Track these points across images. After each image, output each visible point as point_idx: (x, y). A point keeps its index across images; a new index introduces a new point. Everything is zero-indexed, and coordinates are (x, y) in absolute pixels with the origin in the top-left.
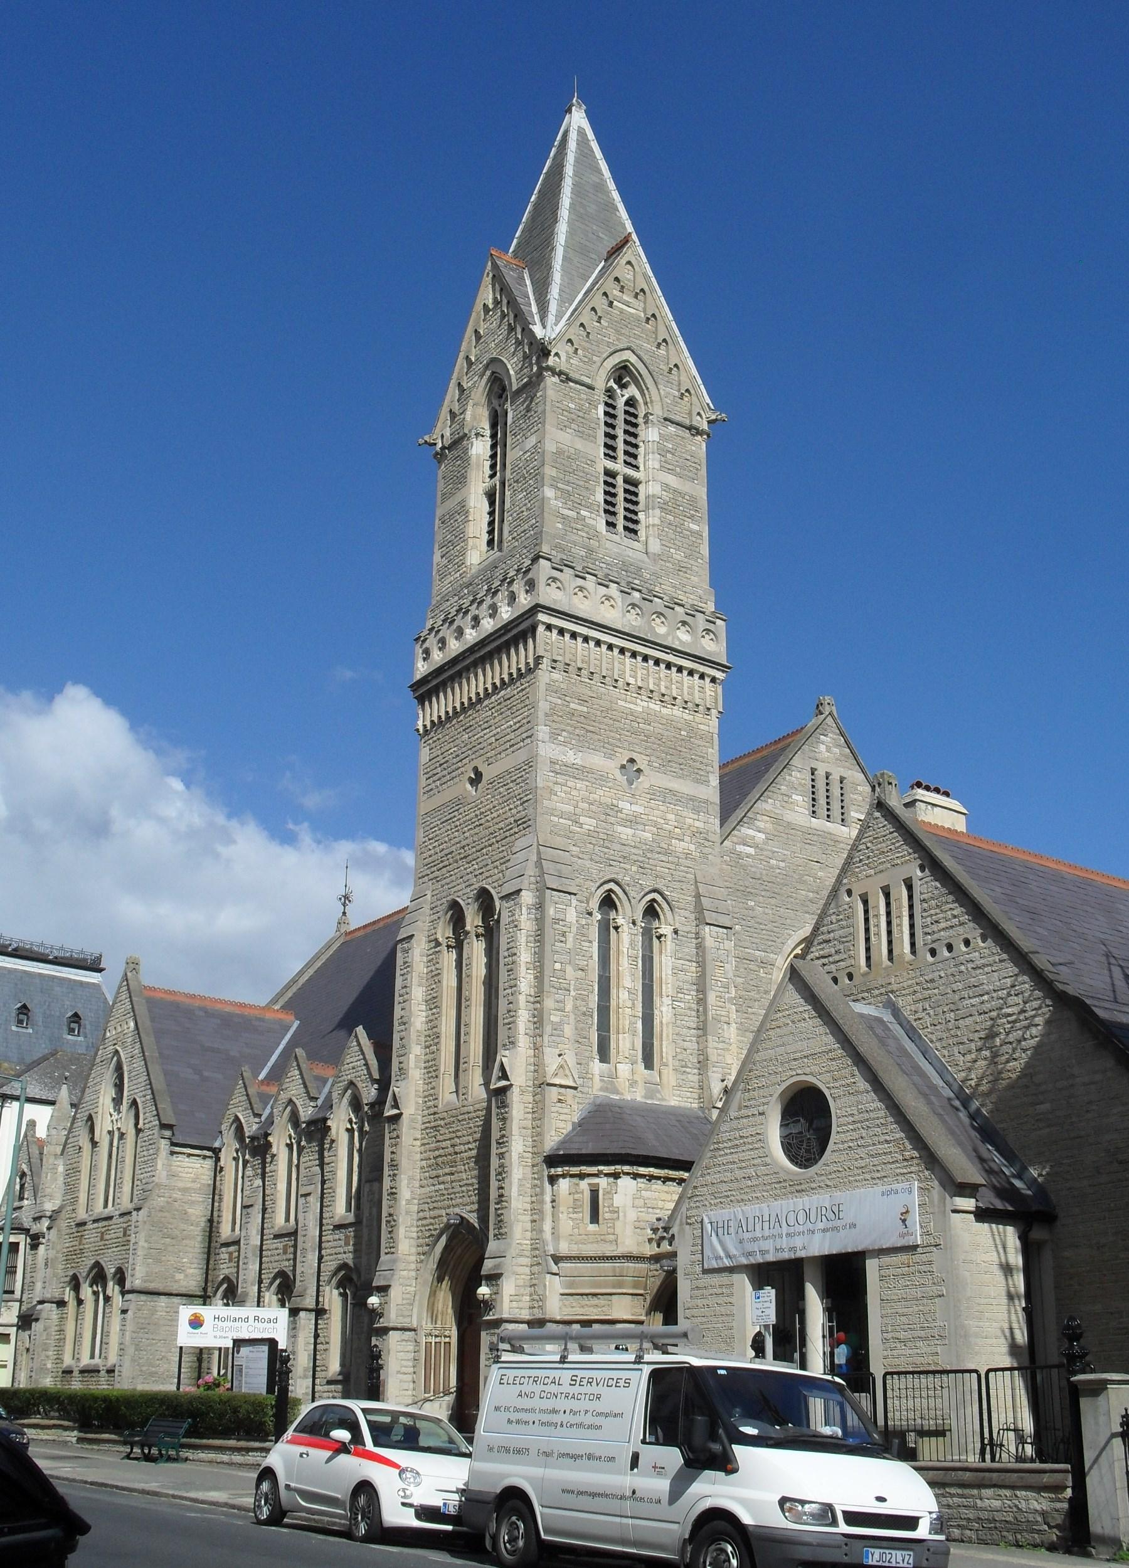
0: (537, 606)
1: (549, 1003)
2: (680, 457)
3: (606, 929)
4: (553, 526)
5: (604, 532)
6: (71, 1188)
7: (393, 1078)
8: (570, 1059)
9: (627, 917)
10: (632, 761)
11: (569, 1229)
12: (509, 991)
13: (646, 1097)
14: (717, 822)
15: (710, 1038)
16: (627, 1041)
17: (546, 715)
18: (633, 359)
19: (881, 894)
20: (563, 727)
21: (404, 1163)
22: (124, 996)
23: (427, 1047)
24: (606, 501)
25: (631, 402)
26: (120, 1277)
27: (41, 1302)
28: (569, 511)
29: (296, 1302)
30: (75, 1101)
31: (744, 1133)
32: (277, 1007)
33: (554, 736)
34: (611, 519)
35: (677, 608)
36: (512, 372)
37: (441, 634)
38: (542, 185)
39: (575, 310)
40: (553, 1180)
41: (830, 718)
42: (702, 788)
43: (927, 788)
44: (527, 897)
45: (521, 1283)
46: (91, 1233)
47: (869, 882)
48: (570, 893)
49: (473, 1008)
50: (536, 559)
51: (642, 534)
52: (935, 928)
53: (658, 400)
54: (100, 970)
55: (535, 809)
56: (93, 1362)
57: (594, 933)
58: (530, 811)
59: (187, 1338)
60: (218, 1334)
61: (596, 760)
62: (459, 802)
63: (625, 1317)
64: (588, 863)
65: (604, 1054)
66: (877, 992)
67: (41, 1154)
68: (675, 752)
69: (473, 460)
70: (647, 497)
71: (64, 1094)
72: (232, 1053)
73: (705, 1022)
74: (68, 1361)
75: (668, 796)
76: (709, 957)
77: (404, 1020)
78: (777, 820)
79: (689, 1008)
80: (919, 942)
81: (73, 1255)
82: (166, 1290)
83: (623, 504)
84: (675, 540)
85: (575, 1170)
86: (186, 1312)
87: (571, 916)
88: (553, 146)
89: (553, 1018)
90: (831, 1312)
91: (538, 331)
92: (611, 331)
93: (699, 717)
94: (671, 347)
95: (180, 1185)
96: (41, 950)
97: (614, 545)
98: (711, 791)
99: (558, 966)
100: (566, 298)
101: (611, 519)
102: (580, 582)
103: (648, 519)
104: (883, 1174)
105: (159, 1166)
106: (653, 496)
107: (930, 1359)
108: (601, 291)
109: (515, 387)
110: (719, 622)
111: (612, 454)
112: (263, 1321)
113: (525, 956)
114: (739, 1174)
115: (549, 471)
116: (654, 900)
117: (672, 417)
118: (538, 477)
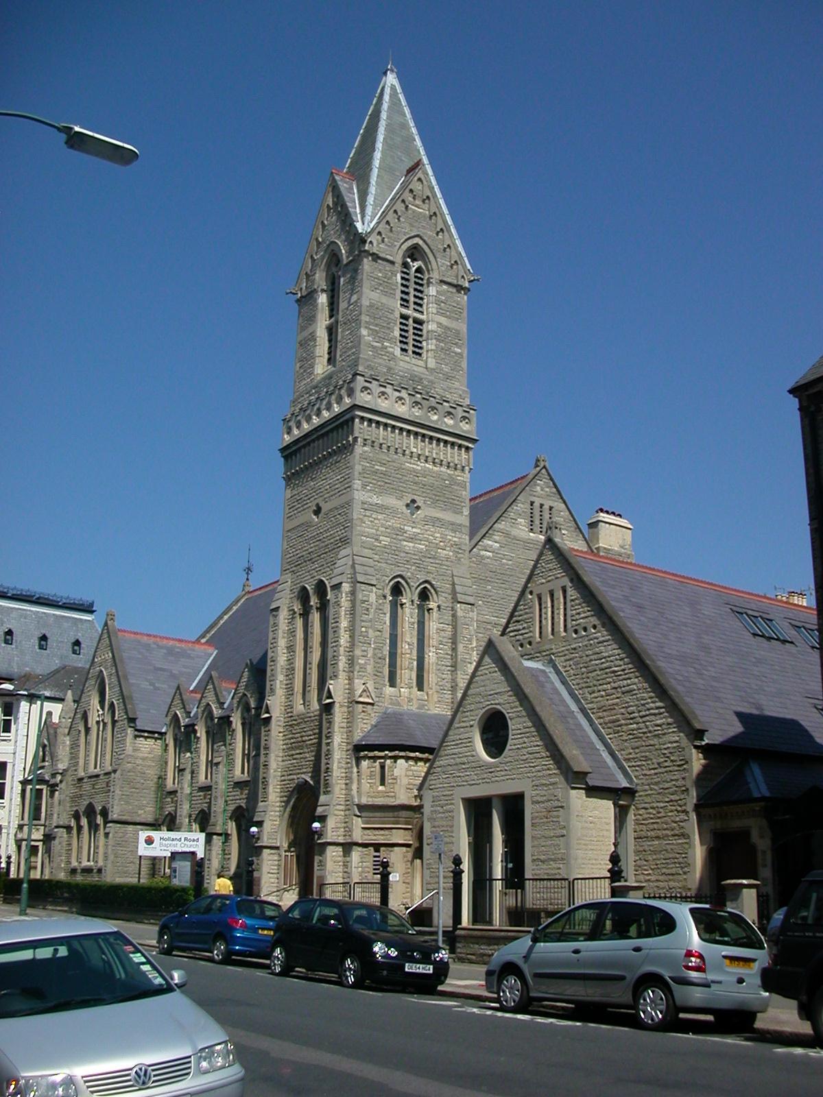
0: (355, 405)
1: (358, 652)
2: (450, 305)
3: (396, 606)
4: (366, 353)
5: (399, 356)
6: (74, 757)
7: (267, 694)
8: (370, 686)
9: (409, 598)
10: (413, 501)
11: (368, 789)
12: (334, 644)
13: (417, 708)
14: (467, 538)
15: (459, 672)
16: (407, 674)
17: (360, 473)
18: (421, 242)
19: (548, 595)
20: (369, 480)
21: (273, 746)
22: (105, 636)
23: (287, 676)
24: (401, 335)
25: (419, 270)
26: (104, 812)
27: (56, 827)
28: (377, 345)
29: (209, 830)
30: (77, 699)
31: (461, 737)
32: (203, 641)
33: (364, 486)
34: (404, 346)
35: (445, 404)
36: (343, 252)
37: (299, 418)
38: (367, 123)
39: (383, 212)
40: (358, 760)
41: (544, 470)
42: (458, 516)
43: (607, 512)
44: (346, 587)
45: (338, 820)
46: (87, 786)
47: (540, 586)
48: (372, 585)
49: (314, 653)
50: (355, 374)
51: (424, 355)
52: (577, 617)
53: (439, 267)
54: (92, 612)
55: (352, 532)
56: (88, 863)
57: (387, 608)
58: (348, 533)
59: (143, 850)
60: (163, 848)
61: (391, 501)
62: (308, 525)
63: (400, 842)
64: (384, 565)
65: (392, 683)
66: (544, 654)
67: (56, 733)
68: (442, 495)
69: (320, 306)
70: (428, 332)
71: (69, 695)
72: (174, 672)
73: (456, 662)
74: (75, 864)
75: (435, 521)
76: (459, 622)
77: (274, 659)
78: (507, 535)
79: (447, 654)
80: (569, 626)
81: (75, 799)
82: (133, 821)
83: (412, 335)
84: (442, 364)
85: (371, 754)
86: (143, 835)
87: (373, 598)
88: (353, 147)
89: (360, 661)
90: (506, 843)
91: (360, 227)
92: (407, 225)
93: (457, 473)
94: (446, 233)
95: (141, 755)
96: (55, 598)
97: (407, 364)
98: (464, 518)
99: (363, 629)
100: (376, 205)
101: (404, 346)
102: (382, 389)
103: (429, 345)
104: (535, 764)
105: (128, 744)
106: (432, 331)
107: (556, 871)
108: (401, 199)
109: (345, 262)
110: (472, 412)
111: (405, 304)
112: (190, 840)
113: (344, 624)
114: (458, 760)
115: (364, 318)
116: (425, 588)
117: (445, 279)
118: (357, 321)
